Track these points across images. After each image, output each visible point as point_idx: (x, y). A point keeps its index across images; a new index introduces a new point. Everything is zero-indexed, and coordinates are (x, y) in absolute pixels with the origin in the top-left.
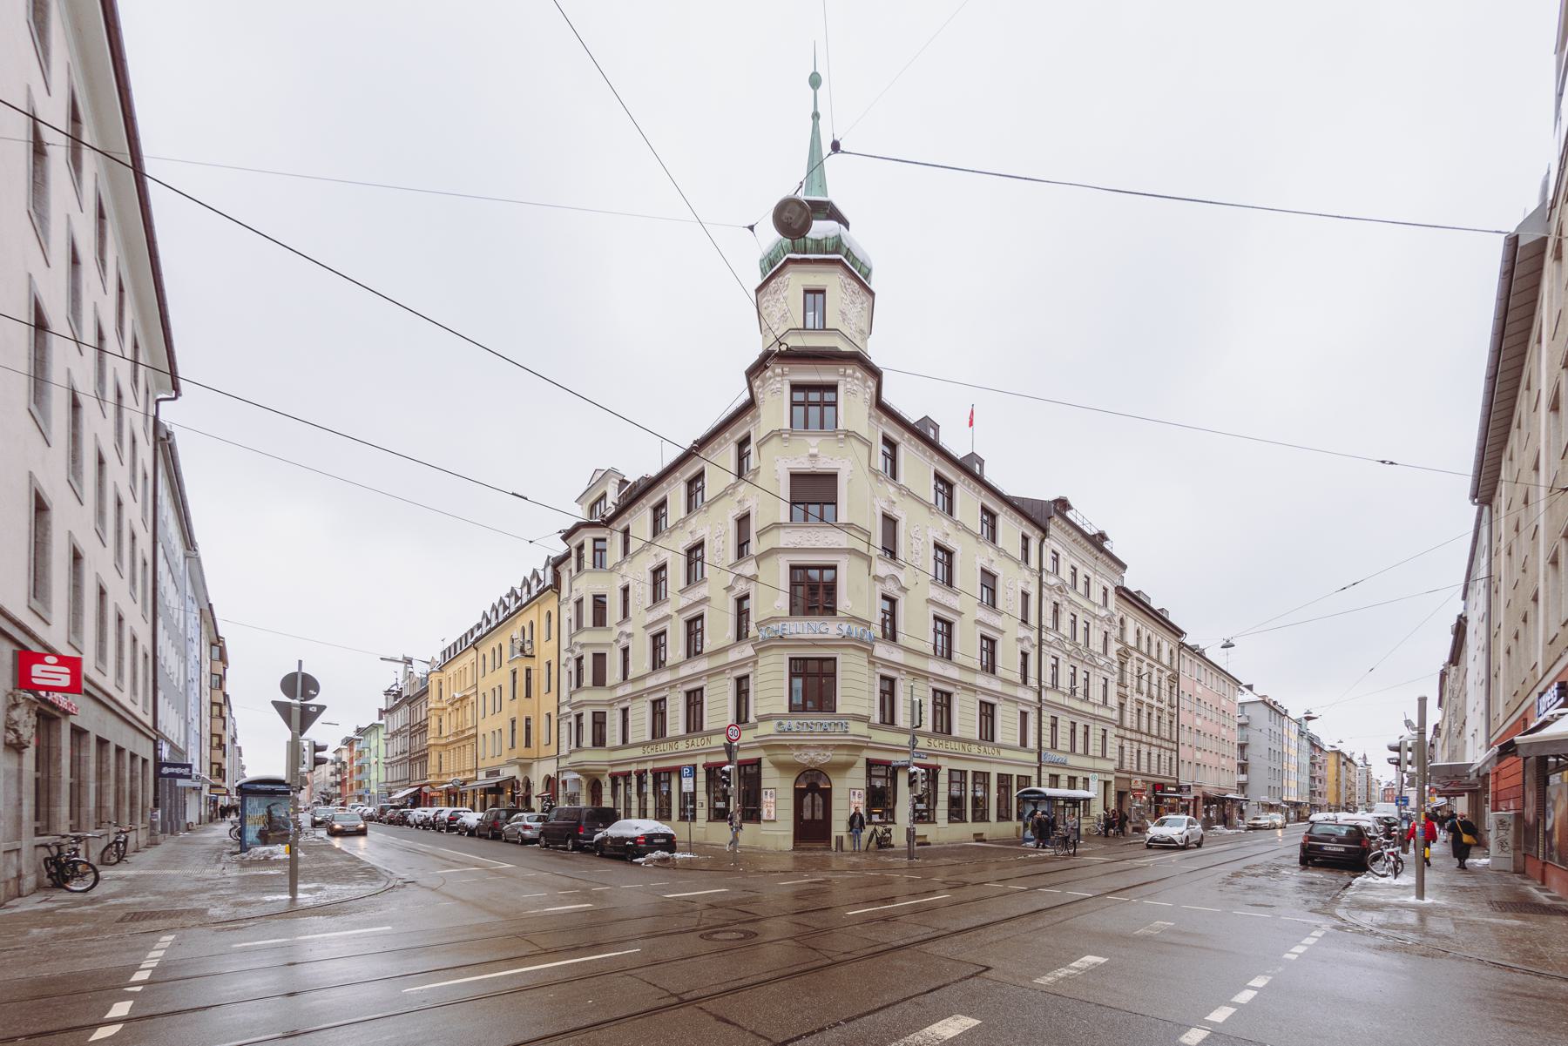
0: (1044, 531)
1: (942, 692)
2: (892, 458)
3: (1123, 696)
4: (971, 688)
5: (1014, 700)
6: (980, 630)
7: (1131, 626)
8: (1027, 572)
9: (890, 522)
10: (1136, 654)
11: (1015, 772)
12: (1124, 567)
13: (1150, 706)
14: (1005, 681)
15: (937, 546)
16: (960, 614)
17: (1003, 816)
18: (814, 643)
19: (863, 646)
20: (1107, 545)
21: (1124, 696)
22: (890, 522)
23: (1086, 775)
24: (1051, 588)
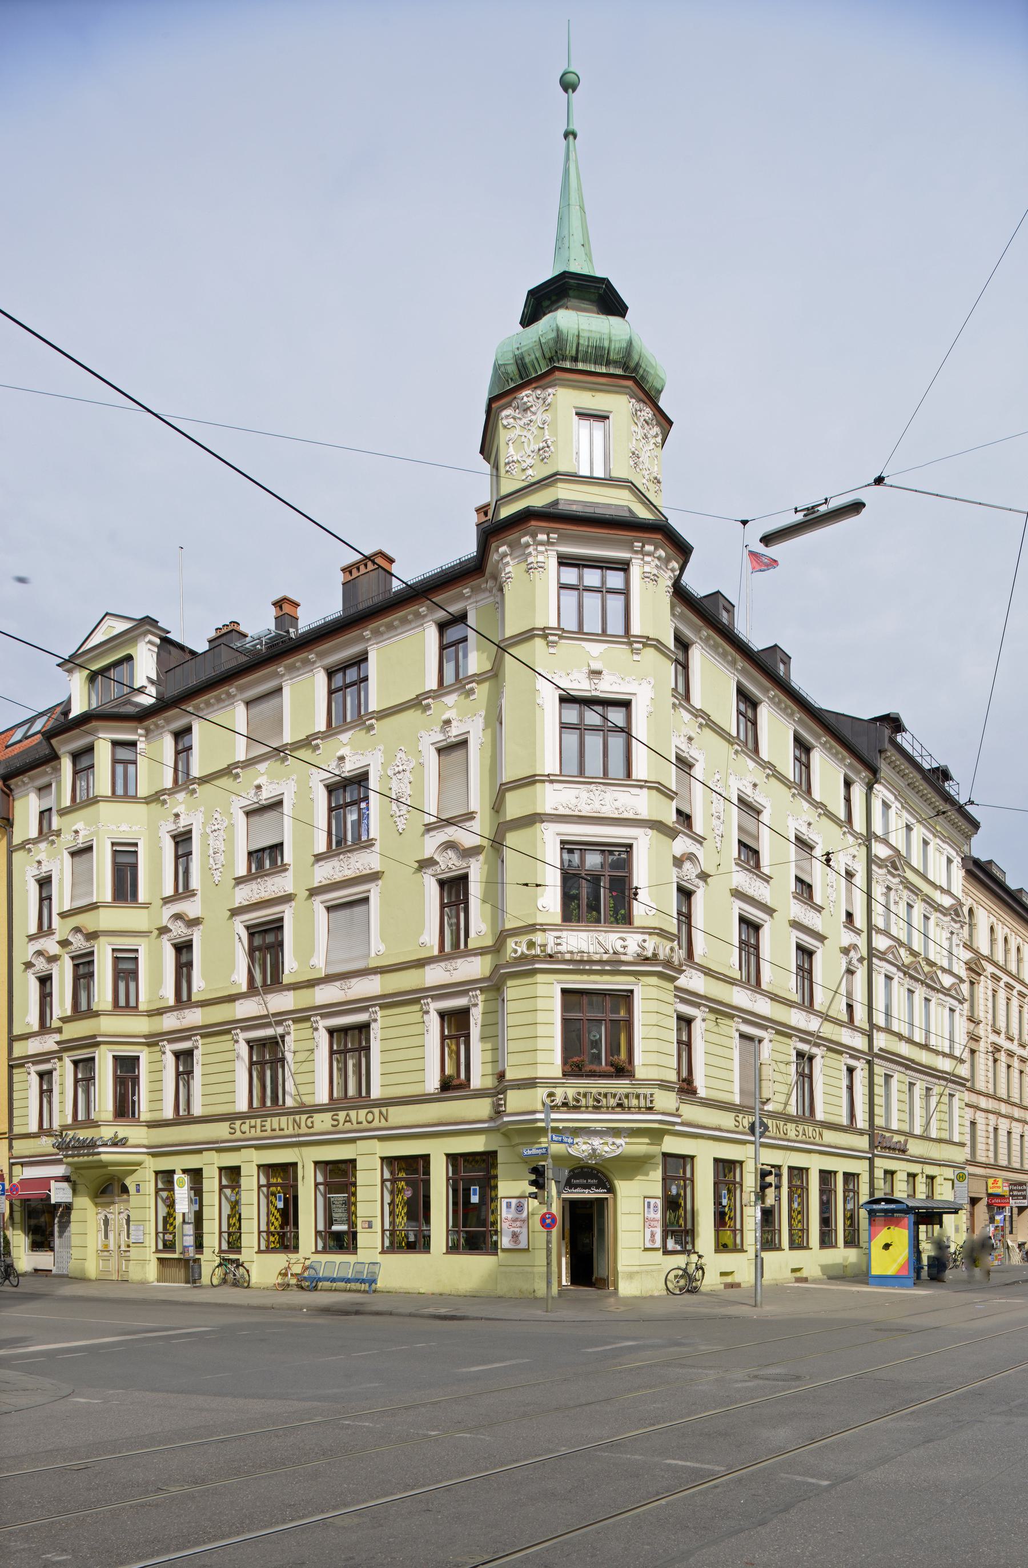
0: (874, 771)
2: (804, 765)
3: (974, 1038)
6: (737, 906)
7: (983, 918)
8: (686, 716)
10: (990, 969)
11: (841, 1166)
12: (975, 825)
13: (1010, 1054)
14: (774, 998)
17: (826, 1240)
18: (614, 965)
19: (668, 971)
20: (949, 787)
21: (974, 1038)
23: (930, 1170)
24: (882, 863)
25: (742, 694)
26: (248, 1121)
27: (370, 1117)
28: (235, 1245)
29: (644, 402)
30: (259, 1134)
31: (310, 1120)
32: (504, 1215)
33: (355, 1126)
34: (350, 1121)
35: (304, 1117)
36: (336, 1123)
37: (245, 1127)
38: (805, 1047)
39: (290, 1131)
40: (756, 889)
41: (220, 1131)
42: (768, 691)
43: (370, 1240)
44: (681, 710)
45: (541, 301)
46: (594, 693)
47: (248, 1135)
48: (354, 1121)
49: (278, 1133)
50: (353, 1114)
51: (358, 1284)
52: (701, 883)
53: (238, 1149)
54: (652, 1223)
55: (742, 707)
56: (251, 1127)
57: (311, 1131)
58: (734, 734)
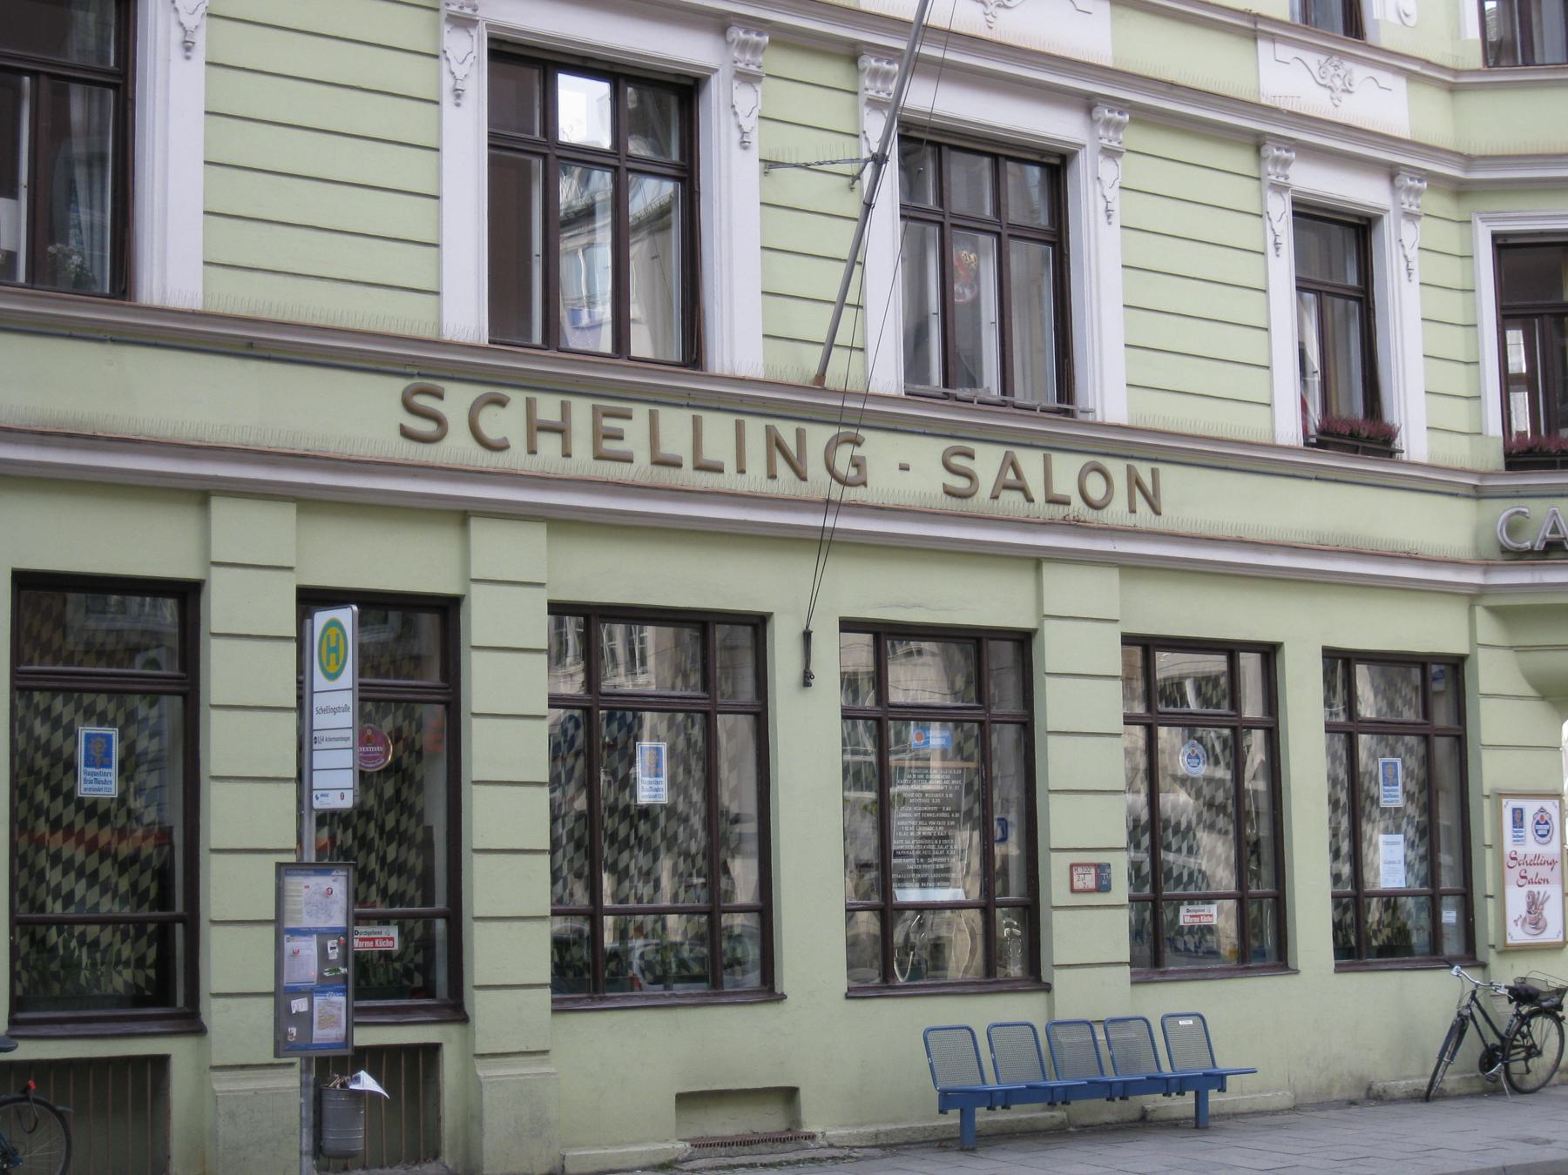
1: (1001, 152)
26: (517, 398)
27: (1096, 486)
28: (417, 969)
30: (582, 461)
31: (844, 455)
32: (1509, 846)
33: (1041, 509)
34: (1023, 489)
35: (818, 436)
36: (961, 483)
37: (506, 422)
39: (755, 479)
41: (358, 416)
43: (1089, 936)
47: (516, 458)
48: (1038, 493)
49: (688, 477)
50: (1030, 463)
51: (1101, 1102)
53: (462, 515)
54: (1531, 872)
56: (536, 428)
57: (853, 494)
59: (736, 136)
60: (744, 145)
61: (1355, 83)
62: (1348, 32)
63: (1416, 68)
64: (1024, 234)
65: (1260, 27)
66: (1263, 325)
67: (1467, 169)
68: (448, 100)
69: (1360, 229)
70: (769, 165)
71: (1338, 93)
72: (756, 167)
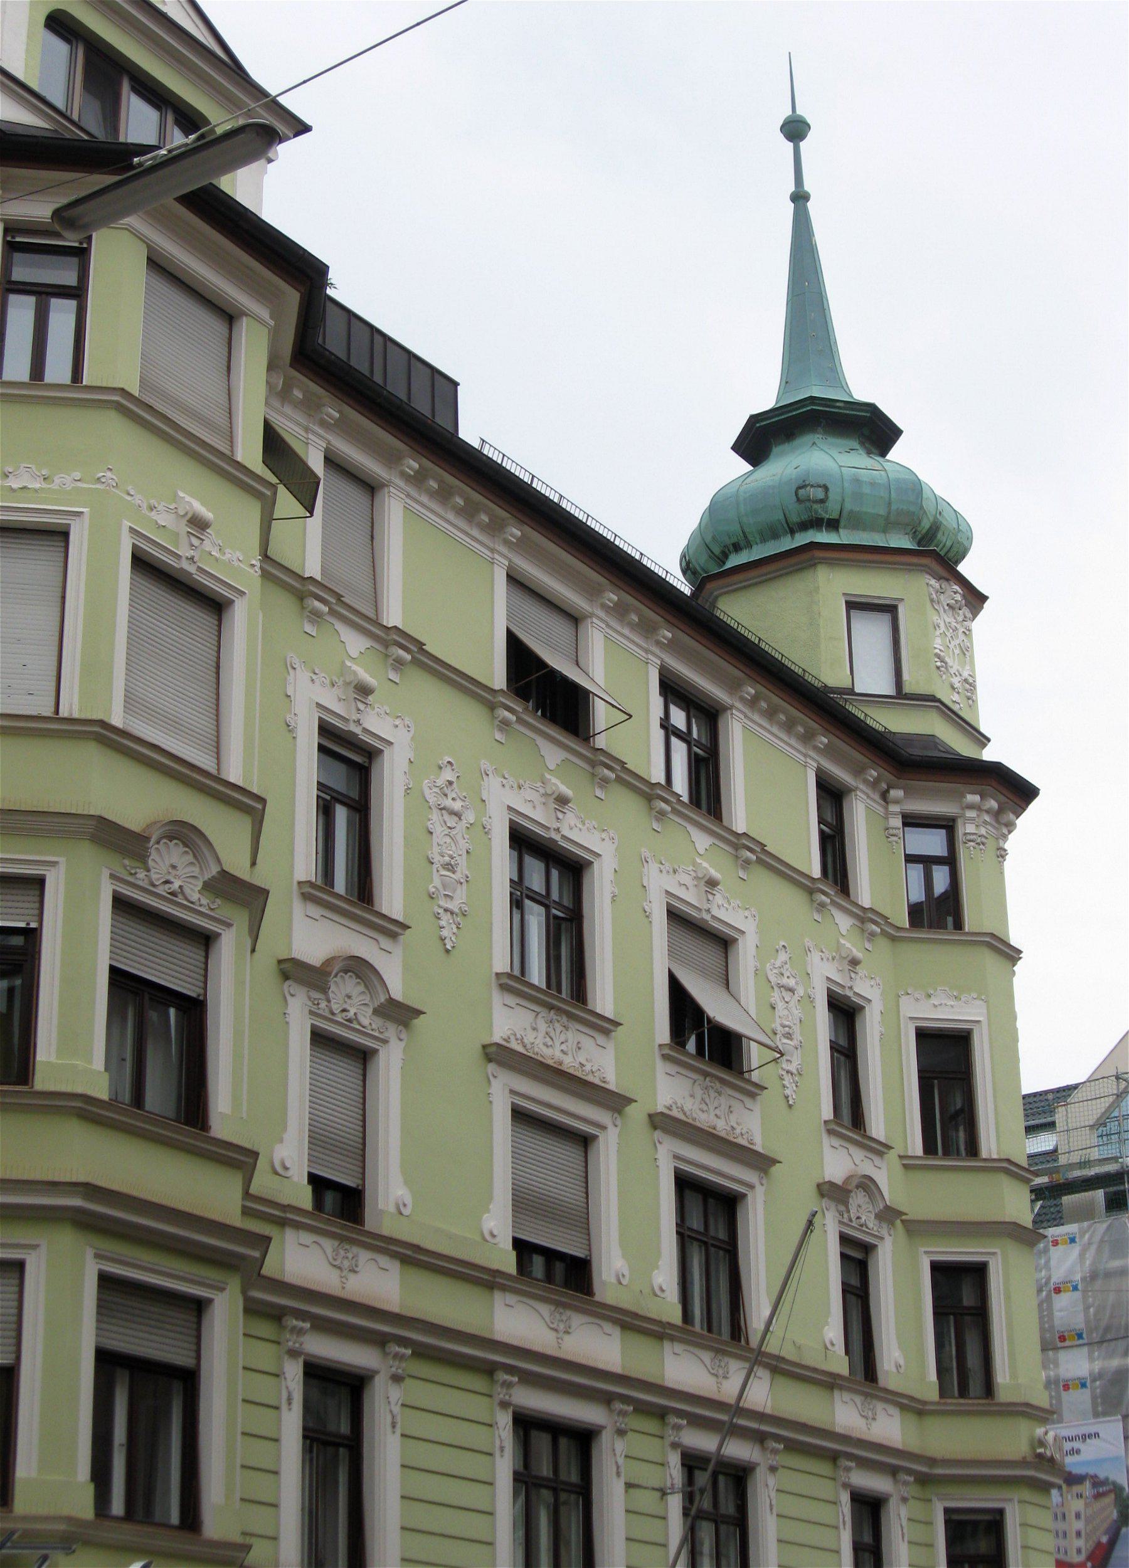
1: (555, 1429)
2: (707, 770)
4: (657, 1406)
5: (829, 1450)
6: (502, 1090)
8: (844, 923)
9: (350, 763)
14: (630, 1322)
15: (523, 841)
16: (762, 1163)
22: (350, 763)
25: (673, 690)
29: (947, 580)
38: (704, 1442)
40: (570, 1046)
42: (318, 407)
44: (339, 626)
45: (758, 439)
46: (353, 728)
52: (391, 1031)
55: (678, 718)
58: (657, 775)
59: (615, 1469)
60: (618, 1474)
61: (361, 1263)
62: (866, 1378)
63: (905, 1401)
64: (570, 1488)
65: (498, 1280)
66: (662, 1541)
67: (931, 1467)
68: (497, 1454)
69: (739, 1477)
70: (629, 1486)
71: (720, 1379)
72: (623, 1486)
